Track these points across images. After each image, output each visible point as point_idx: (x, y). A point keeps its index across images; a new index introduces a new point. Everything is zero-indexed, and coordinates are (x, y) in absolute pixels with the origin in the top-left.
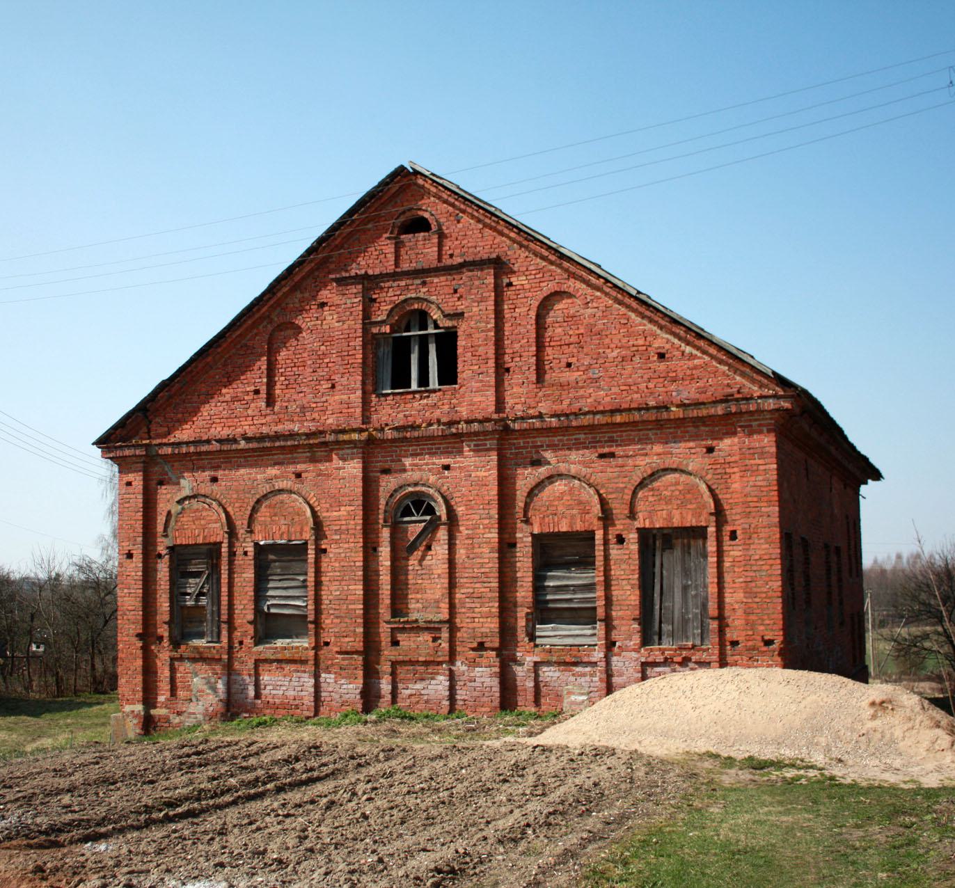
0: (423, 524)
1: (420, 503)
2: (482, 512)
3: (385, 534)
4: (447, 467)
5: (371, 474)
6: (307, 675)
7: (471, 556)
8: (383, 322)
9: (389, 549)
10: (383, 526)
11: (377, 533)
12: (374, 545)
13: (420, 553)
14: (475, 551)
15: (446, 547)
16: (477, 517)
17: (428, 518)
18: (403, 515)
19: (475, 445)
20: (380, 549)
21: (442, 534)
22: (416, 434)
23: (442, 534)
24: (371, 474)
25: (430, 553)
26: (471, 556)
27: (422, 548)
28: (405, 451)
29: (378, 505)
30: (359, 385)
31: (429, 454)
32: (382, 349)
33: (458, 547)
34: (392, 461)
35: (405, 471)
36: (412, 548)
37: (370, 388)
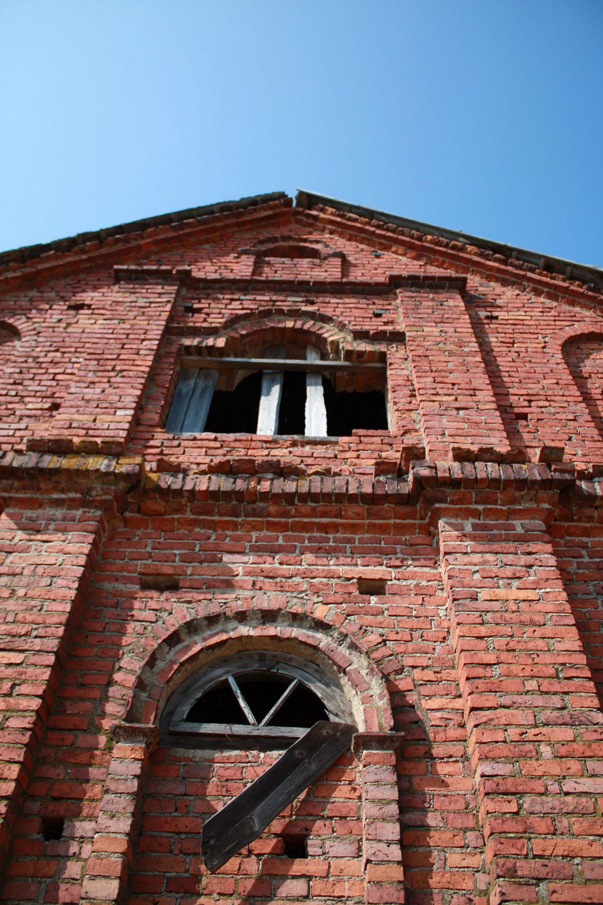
0: (276, 755)
1: (273, 683)
2: (539, 701)
3: (124, 763)
4: (372, 587)
5: (107, 586)
6: (25, 329)
7: (525, 868)
8: (213, 332)
9: (124, 824)
10: (116, 734)
11: (81, 763)
12: (56, 809)
13: (253, 866)
14: (537, 845)
15: (393, 831)
16: (522, 717)
17: (300, 733)
18: (200, 713)
19: (475, 527)
20: (83, 827)
21: (369, 782)
22: (290, 486)
23: (369, 782)
24: (107, 586)
25: (298, 866)
26: (525, 868)
27: (266, 845)
28: (238, 539)
29: (114, 653)
30: (130, 401)
31: (317, 551)
32: (192, 382)
33: (435, 838)
34: (185, 559)
35: (229, 586)
36: (226, 834)
37: (152, 416)
